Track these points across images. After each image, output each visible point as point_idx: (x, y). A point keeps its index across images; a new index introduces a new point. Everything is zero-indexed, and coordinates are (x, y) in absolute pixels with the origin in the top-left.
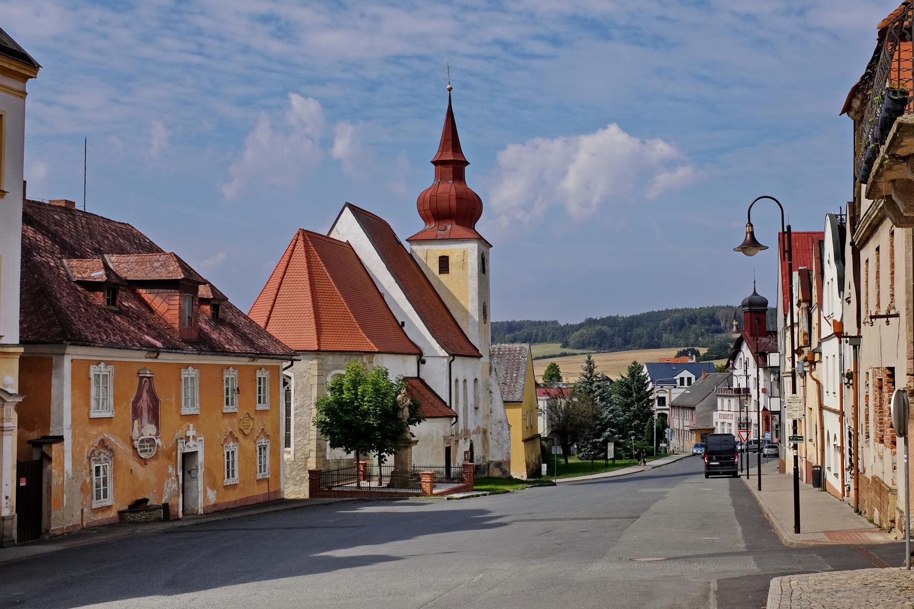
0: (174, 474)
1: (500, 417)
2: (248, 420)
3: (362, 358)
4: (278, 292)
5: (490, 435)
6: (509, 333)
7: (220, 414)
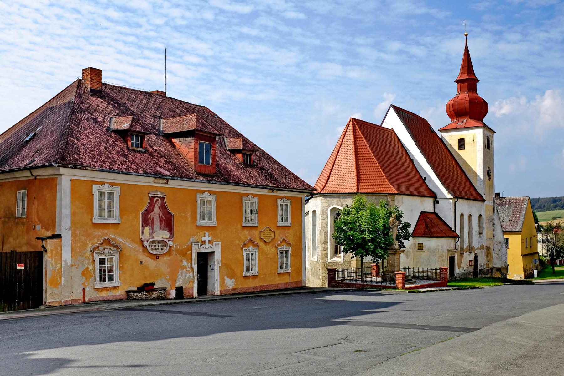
0: (190, 267)
1: (500, 240)
2: (269, 232)
3: (387, 197)
4: (336, 158)
5: (493, 251)
6: (553, 203)
7: (239, 226)
